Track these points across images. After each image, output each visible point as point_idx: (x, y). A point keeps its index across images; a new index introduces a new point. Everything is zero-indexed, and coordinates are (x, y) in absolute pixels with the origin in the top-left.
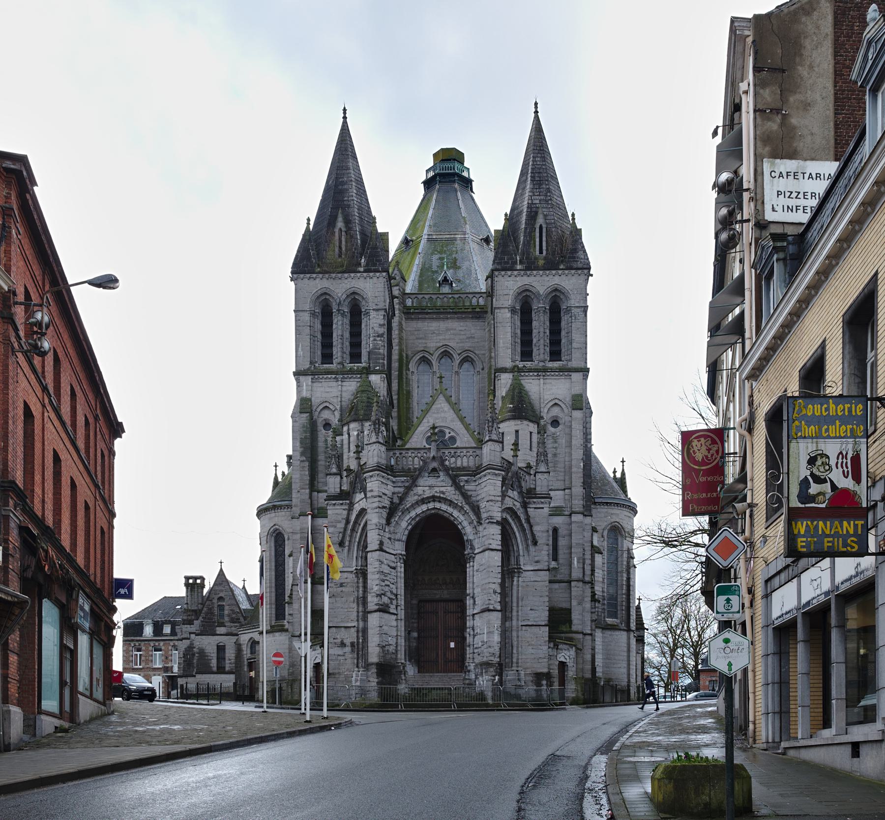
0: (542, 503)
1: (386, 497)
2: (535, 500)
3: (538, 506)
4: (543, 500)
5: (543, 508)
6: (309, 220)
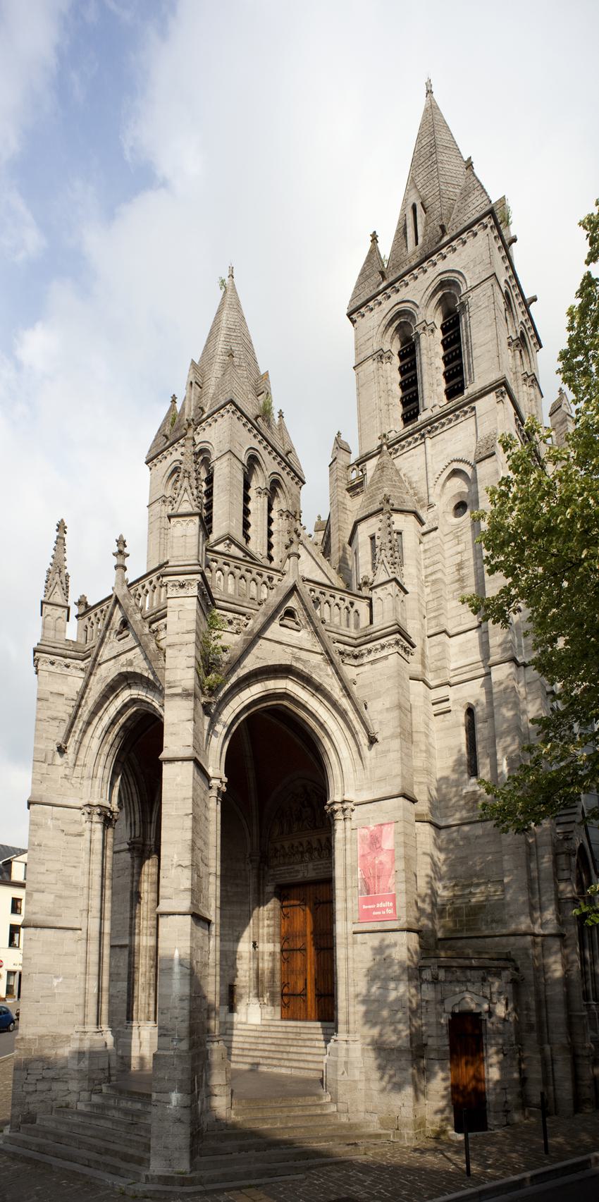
0: (383, 647)
1: (62, 700)
2: (369, 646)
3: (378, 655)
4: (383, 641)
5: (386, 657)
6: (374, 238)
